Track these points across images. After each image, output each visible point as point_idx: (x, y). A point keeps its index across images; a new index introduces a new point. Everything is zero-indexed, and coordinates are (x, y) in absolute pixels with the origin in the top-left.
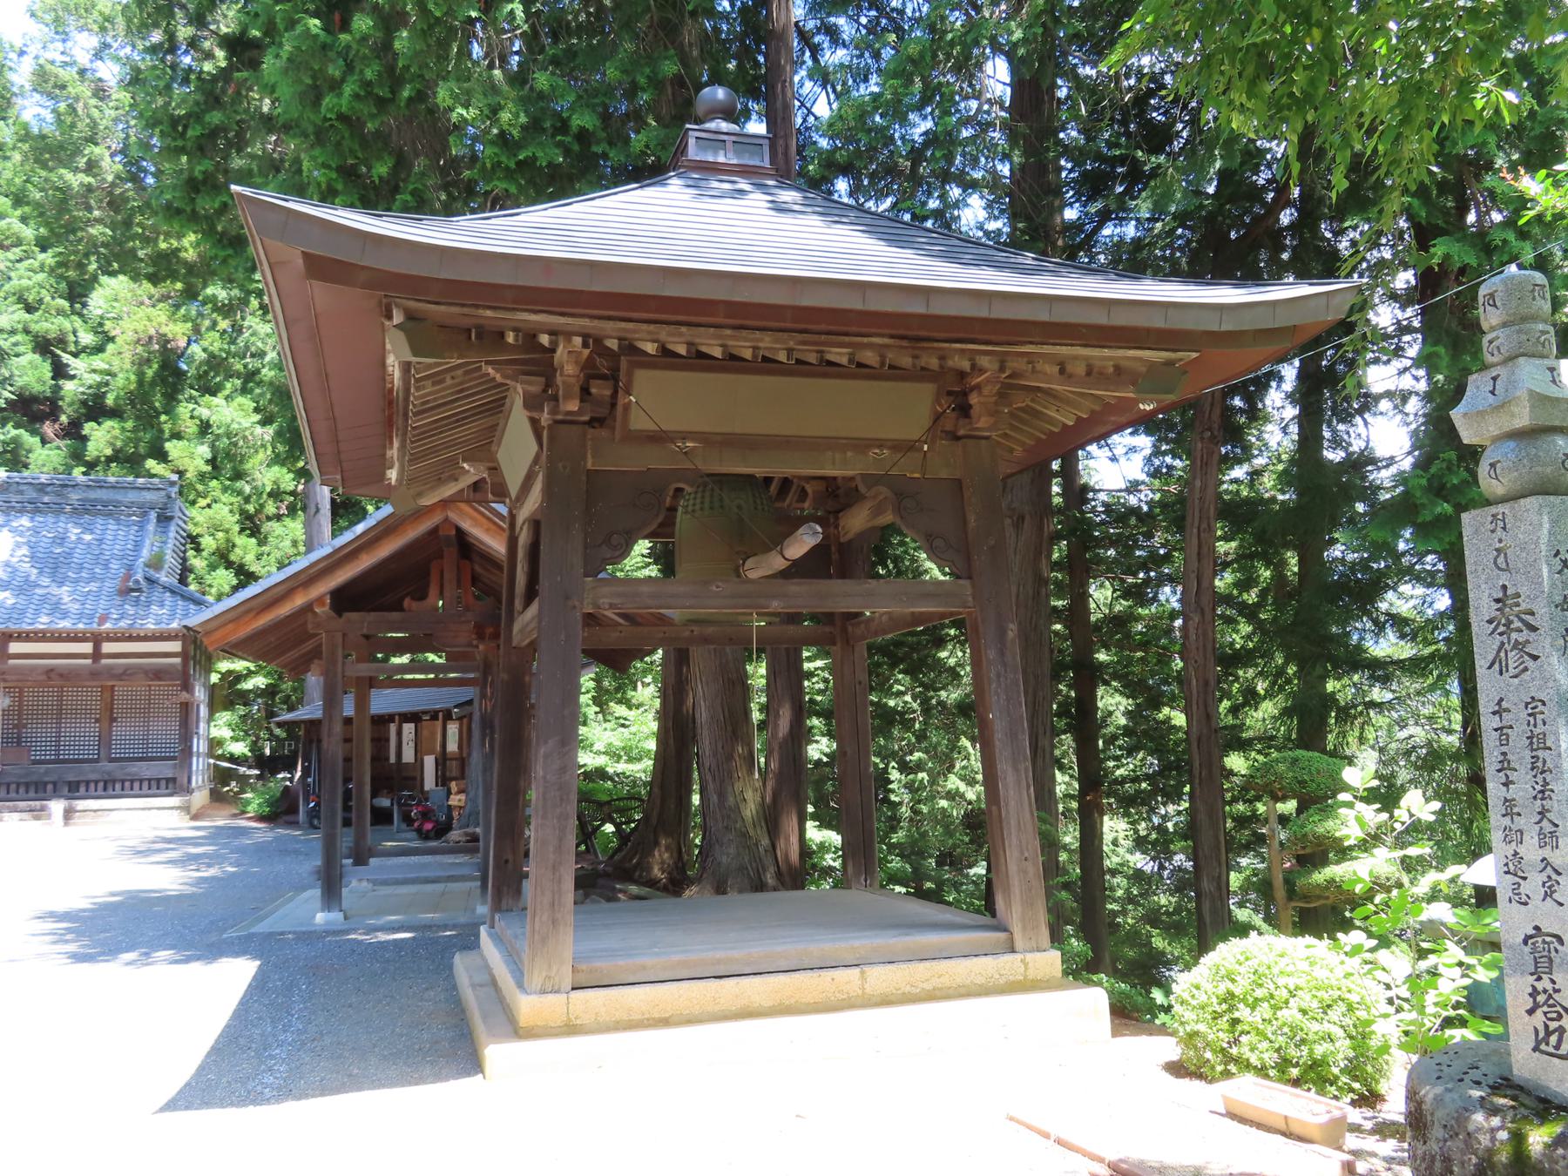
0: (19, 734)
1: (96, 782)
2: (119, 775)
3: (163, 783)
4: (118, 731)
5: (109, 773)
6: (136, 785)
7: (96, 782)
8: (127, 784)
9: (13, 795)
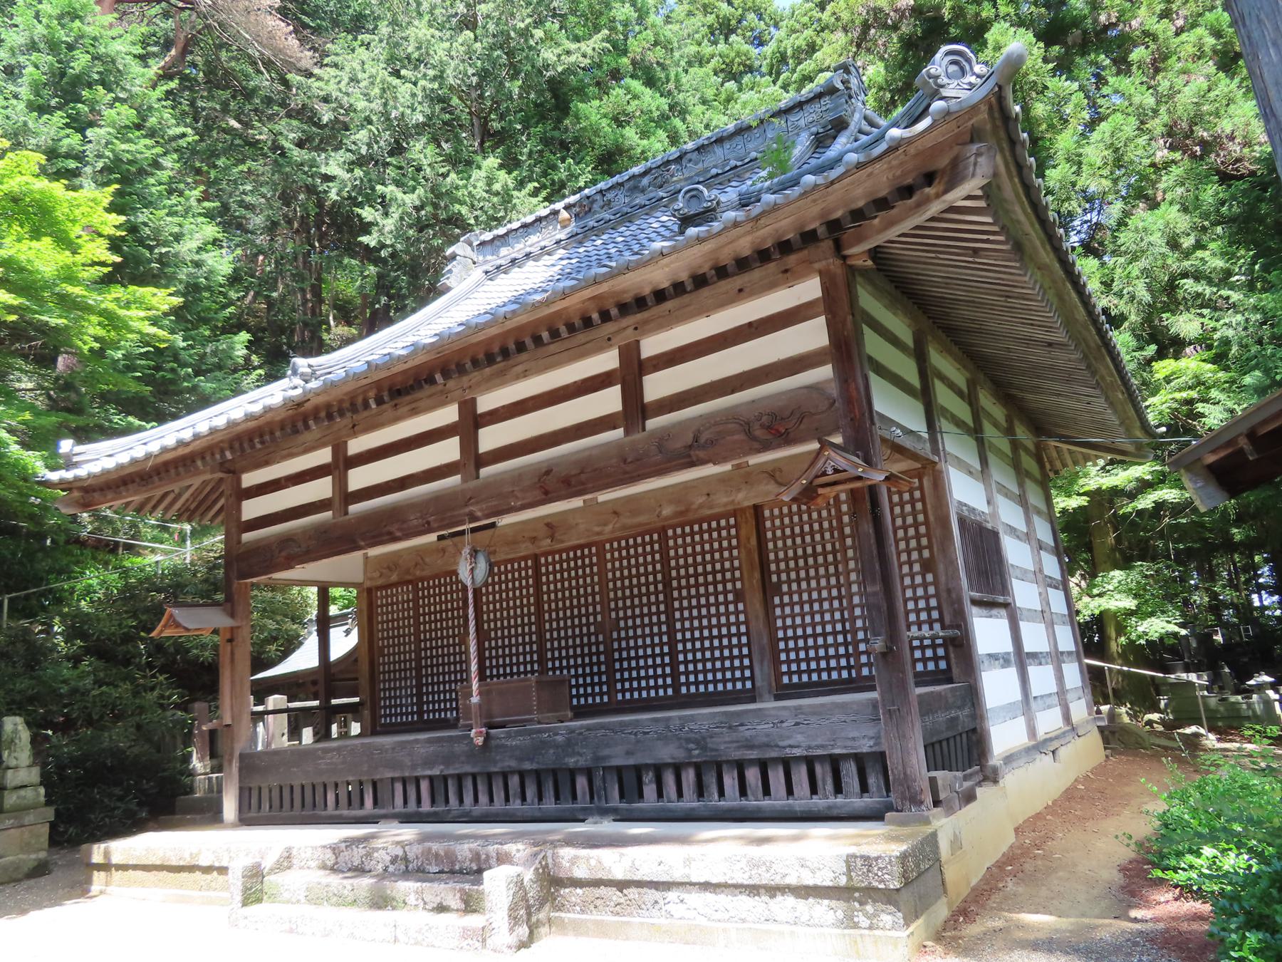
0: (608, 642)
1: (678, 769)
2: (726, 746)
3: (850, 773)
4: (787, 616)
5: (701, 743)
6: (777, 778)
7: (678, 769)
8: (753, 775)
9: (714, 801)
